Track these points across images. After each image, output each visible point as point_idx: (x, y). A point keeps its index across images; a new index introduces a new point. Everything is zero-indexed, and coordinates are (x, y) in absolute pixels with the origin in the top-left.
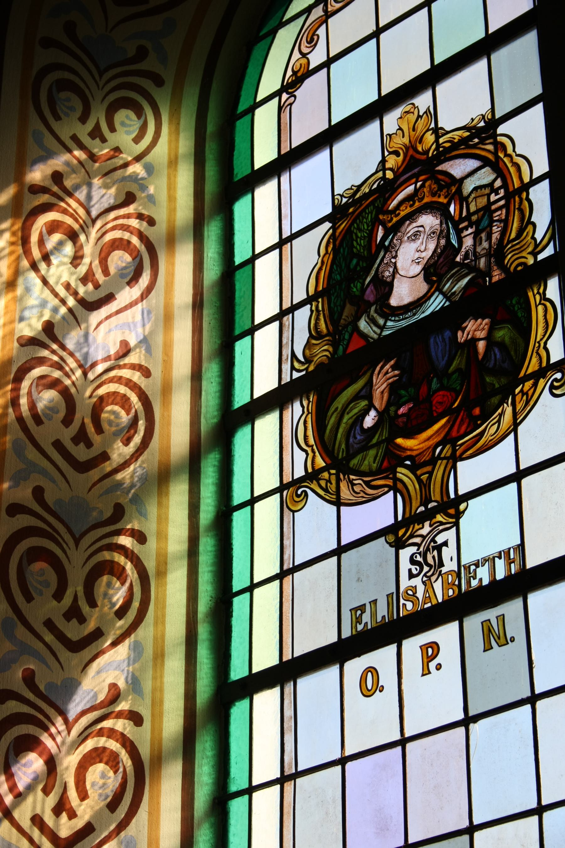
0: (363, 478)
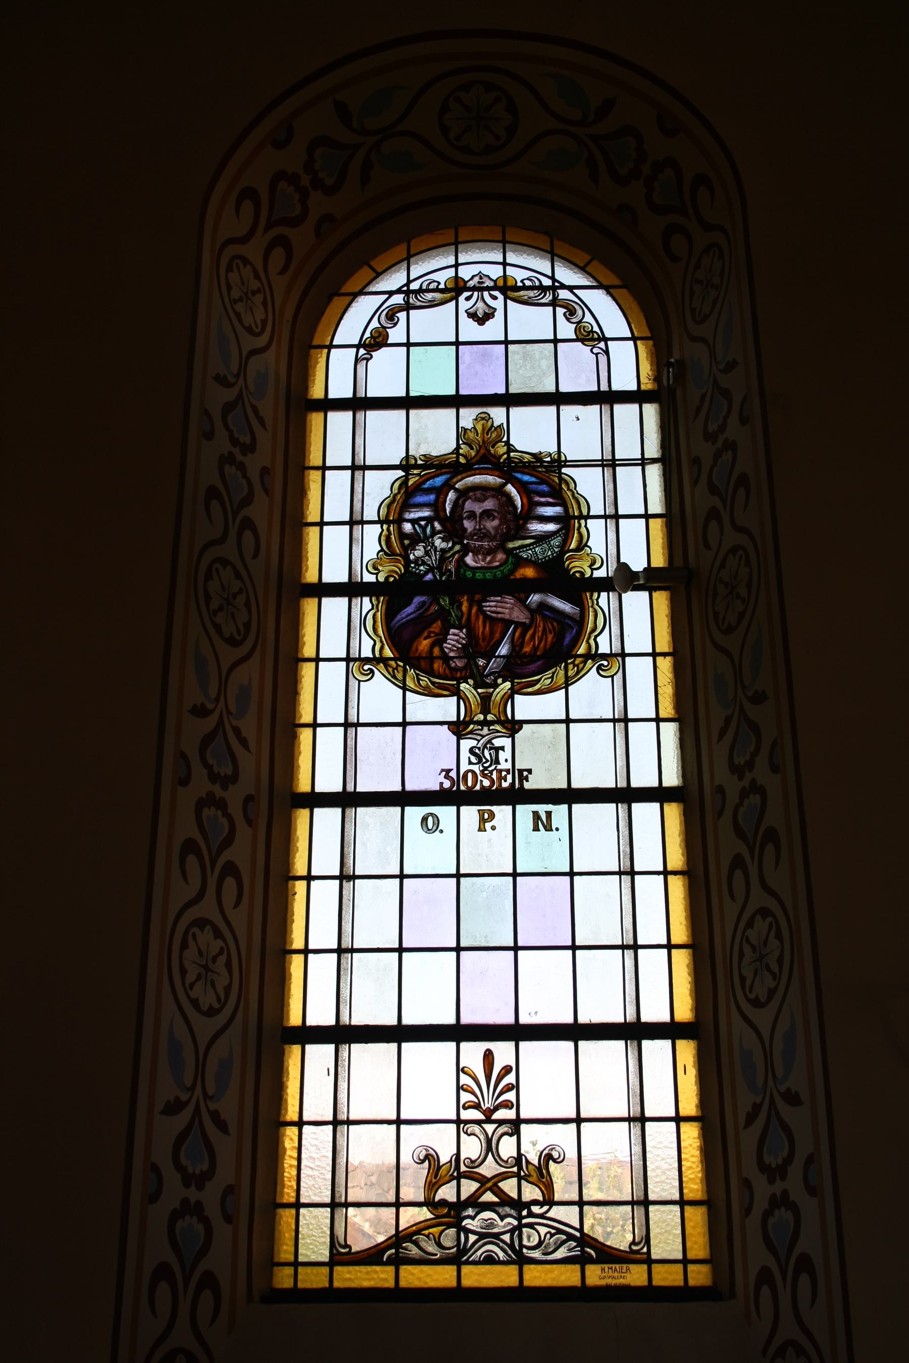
0: (430, 678)
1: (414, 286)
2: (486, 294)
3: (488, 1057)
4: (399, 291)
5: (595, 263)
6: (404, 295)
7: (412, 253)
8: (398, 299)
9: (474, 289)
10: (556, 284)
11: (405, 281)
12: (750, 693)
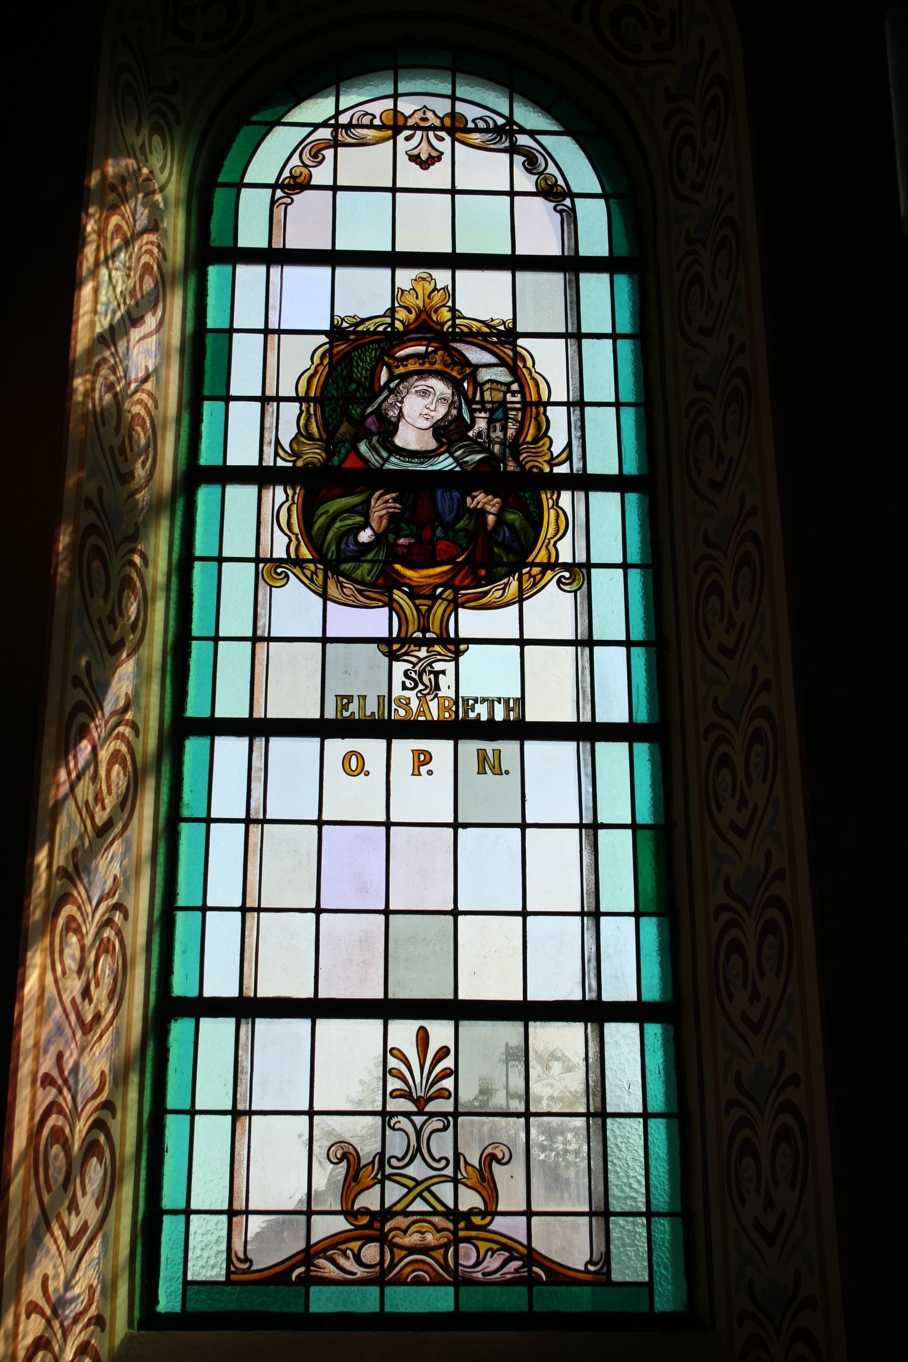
1: (344, 119)
2: (431, 134)
4: (325, 124)
8: (325, 133)
9: (416, 128)
10: (515, 127)
11: (333, 113)
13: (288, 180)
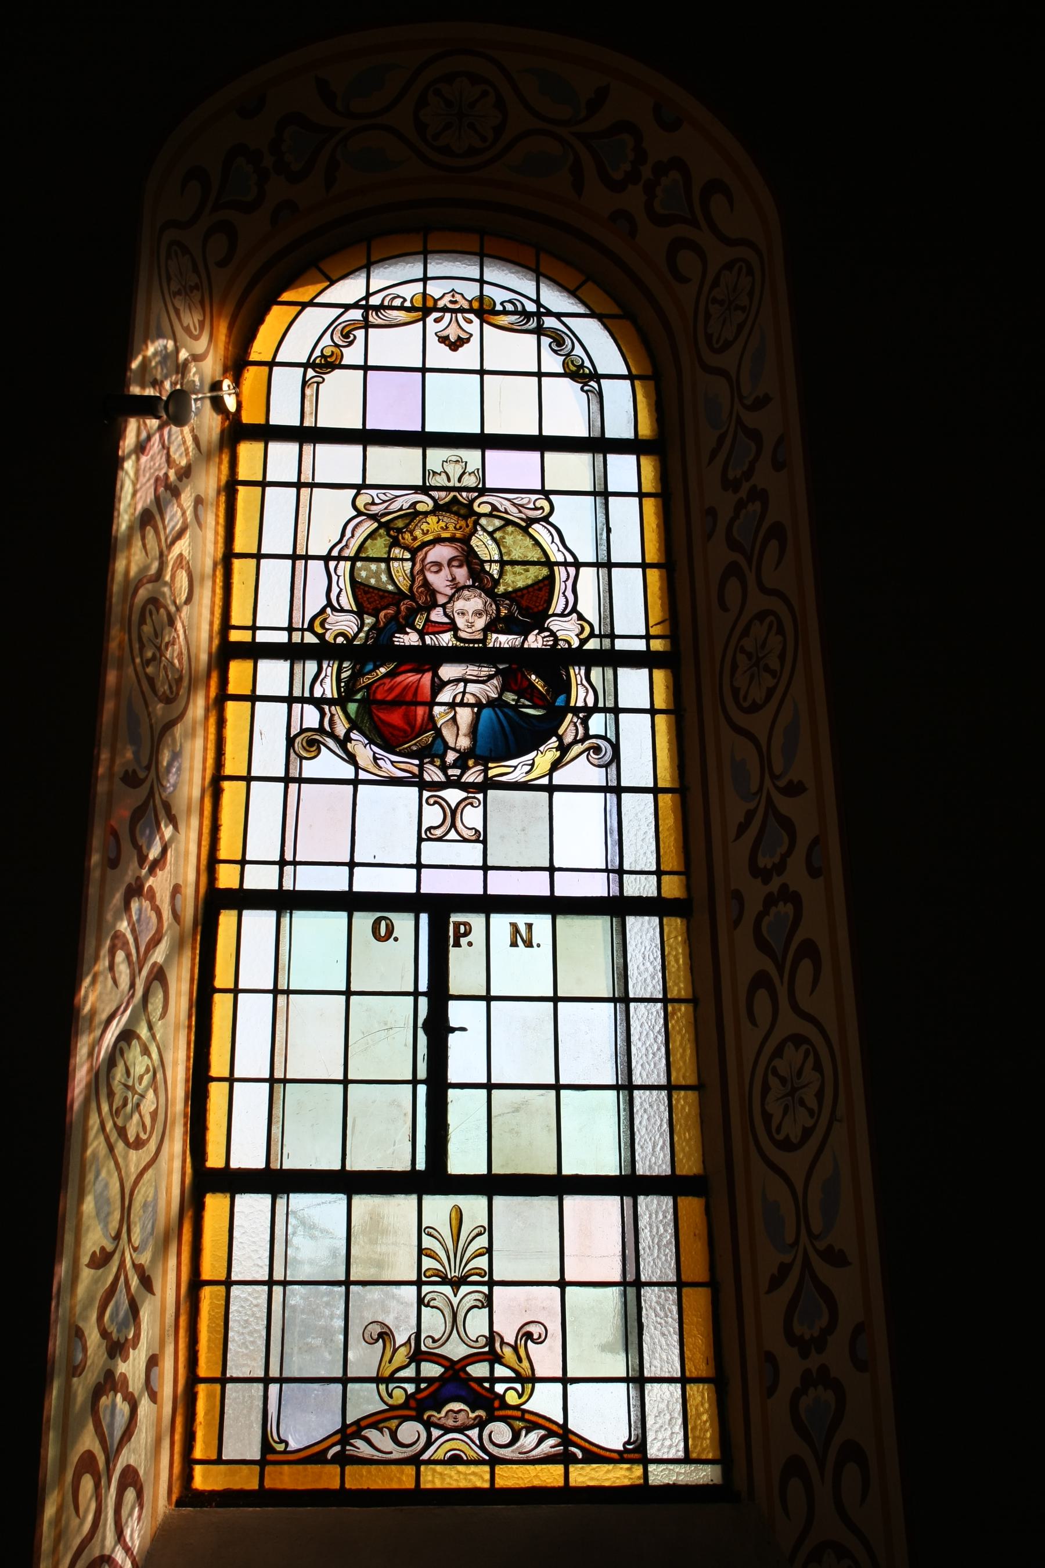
1: (375, 301)
2: (459, 316)
3: (458, 1217)
4: (356, 306)
5: (589, 285)
6: (363, 311)
7: (373, 259)
8: (356, 314)
9: (445, 310)
10: (542, 310)
11: (364, 294)
12: (782, 783)
13: (319, 359)
